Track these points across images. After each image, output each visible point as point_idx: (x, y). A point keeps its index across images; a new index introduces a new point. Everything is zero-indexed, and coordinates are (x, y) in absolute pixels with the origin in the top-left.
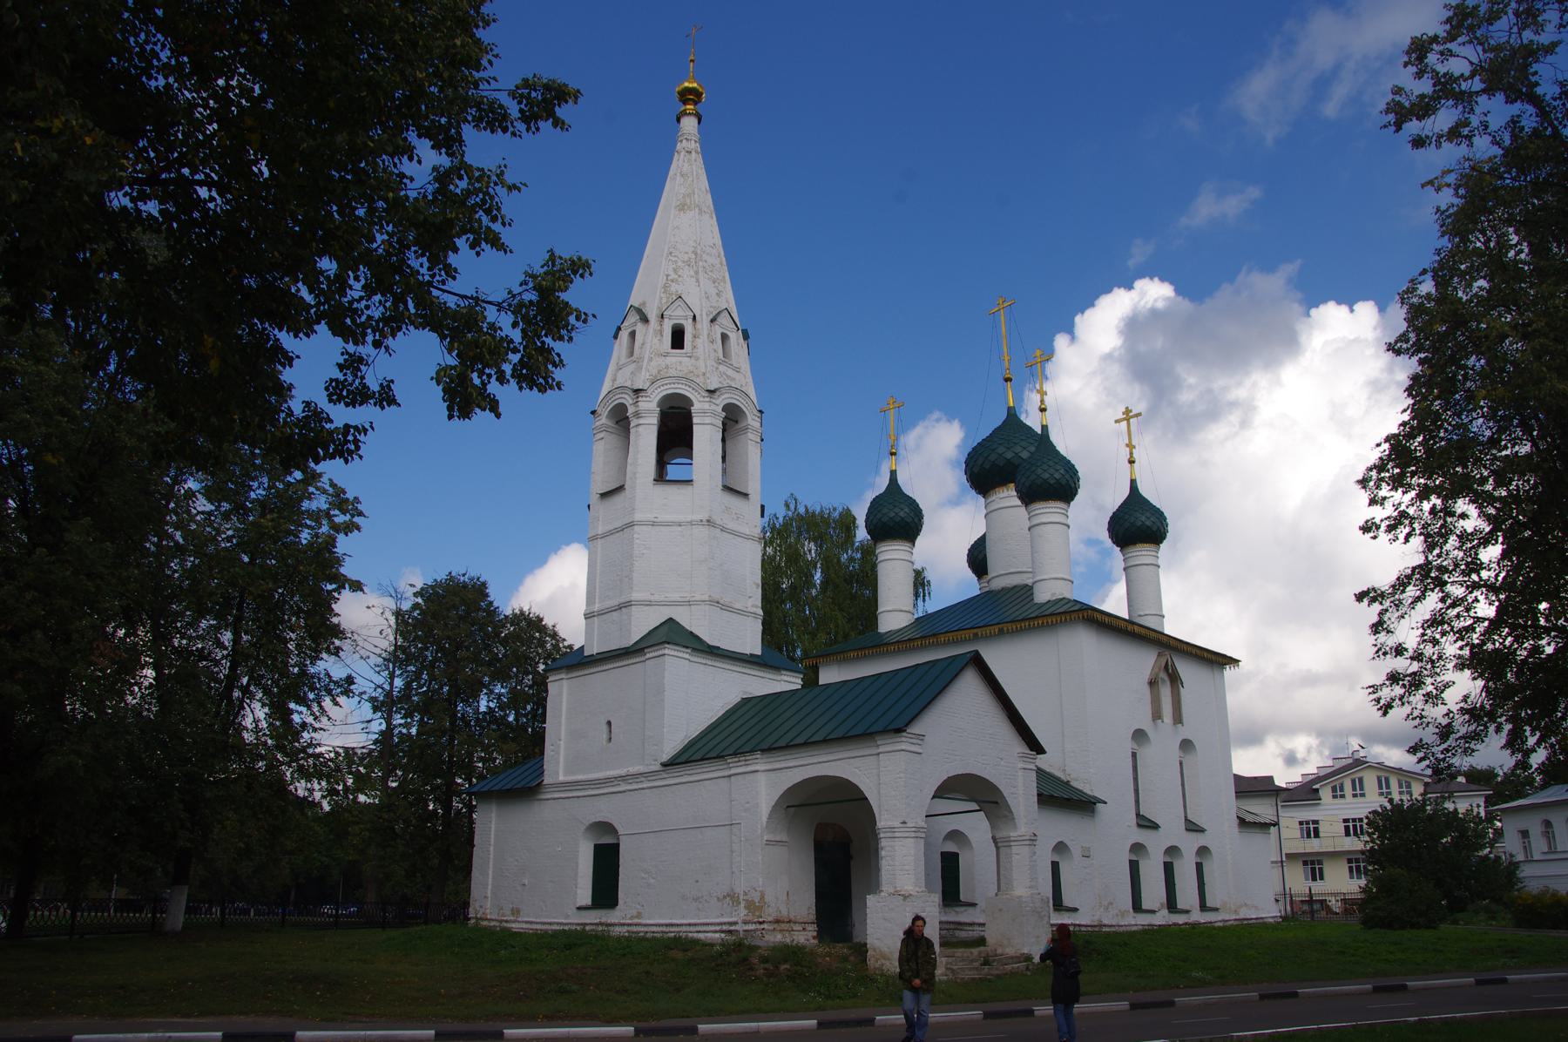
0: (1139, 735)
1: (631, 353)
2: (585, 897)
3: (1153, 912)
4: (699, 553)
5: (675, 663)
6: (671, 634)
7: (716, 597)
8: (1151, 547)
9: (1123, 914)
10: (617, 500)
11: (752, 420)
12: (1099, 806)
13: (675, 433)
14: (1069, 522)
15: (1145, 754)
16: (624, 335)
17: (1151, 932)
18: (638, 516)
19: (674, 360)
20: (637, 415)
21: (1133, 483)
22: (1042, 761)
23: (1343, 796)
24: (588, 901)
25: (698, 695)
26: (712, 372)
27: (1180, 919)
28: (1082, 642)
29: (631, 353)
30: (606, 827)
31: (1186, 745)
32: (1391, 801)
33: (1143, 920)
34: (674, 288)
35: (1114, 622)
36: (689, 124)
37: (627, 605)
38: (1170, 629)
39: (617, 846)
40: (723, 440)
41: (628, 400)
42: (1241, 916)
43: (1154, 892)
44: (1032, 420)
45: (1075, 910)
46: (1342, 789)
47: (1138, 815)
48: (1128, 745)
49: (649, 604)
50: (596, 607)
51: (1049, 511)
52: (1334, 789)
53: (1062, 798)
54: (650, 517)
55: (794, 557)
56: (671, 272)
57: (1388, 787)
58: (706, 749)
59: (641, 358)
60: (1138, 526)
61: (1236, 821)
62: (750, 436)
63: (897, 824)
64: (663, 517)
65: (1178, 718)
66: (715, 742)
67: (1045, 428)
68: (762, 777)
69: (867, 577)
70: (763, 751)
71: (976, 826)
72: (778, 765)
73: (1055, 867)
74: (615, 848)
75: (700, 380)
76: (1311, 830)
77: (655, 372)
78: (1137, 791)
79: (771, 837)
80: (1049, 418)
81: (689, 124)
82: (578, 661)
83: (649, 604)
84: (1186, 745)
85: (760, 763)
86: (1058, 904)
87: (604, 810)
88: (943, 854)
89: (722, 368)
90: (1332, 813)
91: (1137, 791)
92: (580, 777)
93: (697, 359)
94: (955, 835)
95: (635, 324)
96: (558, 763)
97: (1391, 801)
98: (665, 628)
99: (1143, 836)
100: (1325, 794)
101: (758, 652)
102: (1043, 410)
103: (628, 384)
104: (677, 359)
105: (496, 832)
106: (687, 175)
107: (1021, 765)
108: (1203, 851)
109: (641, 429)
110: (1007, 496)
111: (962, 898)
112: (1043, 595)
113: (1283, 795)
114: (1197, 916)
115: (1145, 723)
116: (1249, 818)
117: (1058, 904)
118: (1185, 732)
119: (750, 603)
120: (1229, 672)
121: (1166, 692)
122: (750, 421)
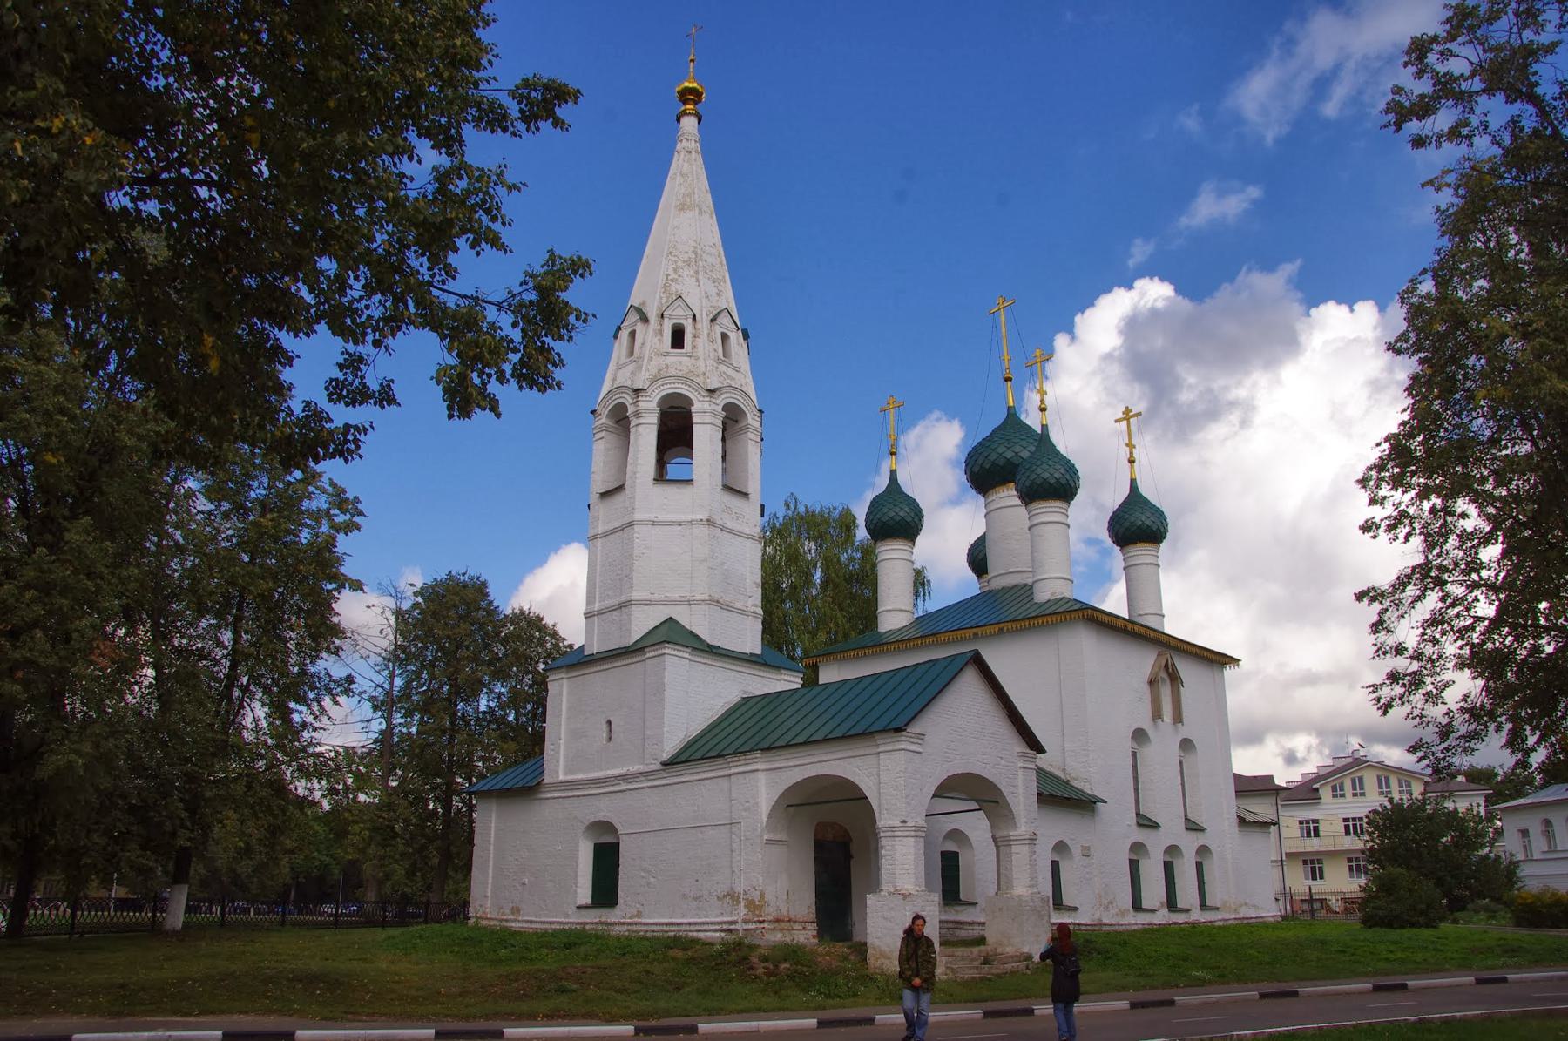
0: (1139, 735)
1: (631, 353)
2: (584, 894)
3: (1153, 911)
4: (699, 551)
5: (676, 665)
6: (671, 634)
7: (716, 596)
8: (1151, 546)
9: (1123, 913)
10: (618, 499)
11: (752, 420)
13: (675, 433)
14: (1069, 521)
15: (1148, 753)
20: (637, 414)
21: (1133, 482)
22: (1042, 760)
23: (1343, 796)
24: (588, 901)
25: (696, 696)
26: (715, 371)
27: (1180, 918)
28: (1083, 644)
29: (631, 353)
30: (605, 826)
31: (1186, 745)
32: (1391, 800)
33: (1143, 919)
36: (689, 123)
37: (628, 604)
38: (1172, 628)
40: (723, 439)
41: (628, 399)
43: (1154, 892)
44: (1032, 420)
45: (1076, 909)
46: (1342, 789)
47: (1138, 814)
48: (1128, 745)
49: (649, 603)
50: (597, 606)
51: (1048, 510)
52: (1334, 789)
53: (1062, 797)
56: (671, 271)
57: (1388, 786)
59: (642, 358)
60: (1138, 526)
61: (1236, 820)
62: (750, 435)
63: (897, 823)
64: (662, 517)
65: (1178, 718)
67: (1044, 427)
68: (762, 778)
69: (867, 577)
71: (976, 826)
73: (1055, 865)
74: (615, 848)
76: (1311, 829)
77: (654, 371)
78: (1136, 790)
81: (689, 123)
82: (579, 661)
83: (649, 603)
84: (1186, 745)
85: (760, 763)
87: (603, 809)
88: (943, 854)
89: (722, 368)
90: (1332, 812)
91: (1136, 790)
92: (580, 776)
94: (956, 835)
95: (635, 324)
96: (559, 762)
97: (1391, 800)
100: (1325, 793)
102: (1043, 410)
103: (628, 383)
106: (687, 173)
107: (1021, 764)
108: (1203, 850)
109: (641, 428)
112: (1043, 594)
113: (1283, 795)
114: (1197, 916)
115: (1146, 724)
116: (1249, 817)
118: (1185, 731)
119: (750, 602)
120: (1229, 672)
122: (750, 421)
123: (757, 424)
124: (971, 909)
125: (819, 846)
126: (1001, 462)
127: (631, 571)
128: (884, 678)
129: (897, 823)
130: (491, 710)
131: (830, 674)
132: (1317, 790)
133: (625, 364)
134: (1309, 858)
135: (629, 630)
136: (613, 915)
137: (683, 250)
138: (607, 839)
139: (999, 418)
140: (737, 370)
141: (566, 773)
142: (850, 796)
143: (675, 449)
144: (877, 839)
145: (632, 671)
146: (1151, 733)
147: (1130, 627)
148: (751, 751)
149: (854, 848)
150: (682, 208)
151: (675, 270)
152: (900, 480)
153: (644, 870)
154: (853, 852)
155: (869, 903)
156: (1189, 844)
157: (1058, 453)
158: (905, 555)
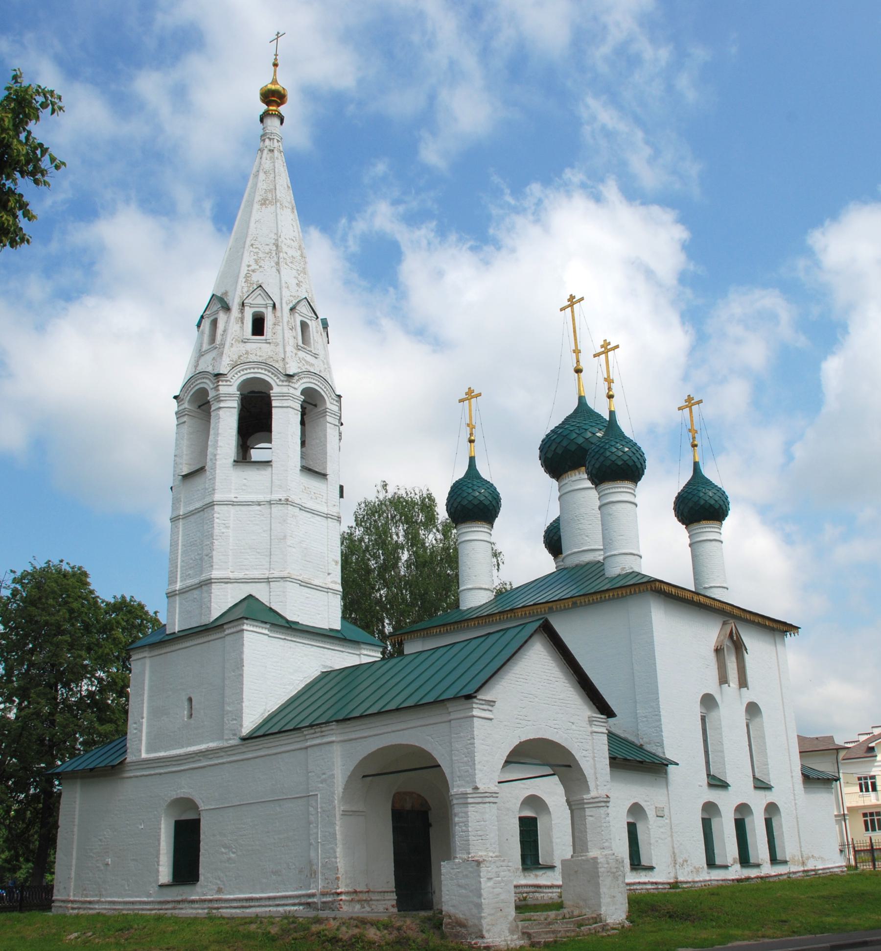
0: (708, 702)
1: (213, 339)
2: (165, 873)
3: (726, 867)
5: (256, 641)
6: (252, 611)
9: (698, 871)
10: (198, 483)
12: (671, 768)
14: (636, 501)
17: (715, 892)
18: (217, 497)
19: (254, 346)
20: (218, 399)
22: (618, 725)
25: (272, 674)
27: (753, 873)
29: (213, 339)
30: (187, 803)
31: (753, 709)
33: (717, 875)
34: (256, 278)
35: (681, 593)
37: (208, 582)
40: (303, 423)
41: (209, 385)
42: (810, 866)
43: (728, 848)
44: (601, 408)
45: (651, 868)
47: (709, 775)
48: (697, 710)
49: (227, 581)
50: (178, 586)
51: (619, 491)
54: (231, 496)
55: (382, 538)
56: (252, 263)
58: (283, 723)
59: (223, 345)
62: (329, 419)
63: (469, 790)
64: (243, 498)
65: (743, 683)
66: (291, 716)
67: (612, 413)
68: (337, 749)
69: (450, 557)
70: (337, 721)
71: (551, 790)
72: (353, 736)
75: (279, 365)
77: (235, 357)
79: (347, 808)
80: (617, 405)
82: (167, 640)
83: (227, 581)
85: (334, 734)
86: (636, 863)
87: (185, 788)
88: (521, 819)
89: (301, 354)
92: (162, 754)
93: (277, 345)
94: (533, 801)
95: (217, 312)
96: (141, 743)
99: (715, 796)
101: (337, 625)
102: (610, 397)
103: (210, 369)
104: (258, 349)
105: (78, 810)
108: (772, 809)
109: (221, 412)
110: (580, 480)
111: (717, 863)
114: (767, 870)
115: (712, 687)
116: (813, 775)
117: (636, 863)
118: (749, 696)
119: (329, 579)
122: (328, 405)
124: (550, 873)
125: (398, 816)
126: (573, 448)
127: (212, 550)
129: (469, 790)
130: (91, 694)
132: (872, 749)
133: (207, 351)
134: (868, 811)
135: (209, 608)
136: (194, 893)
138: (189, 816)
139: (572, 406)
141: (148, 751)
142: (427, 766)
143: (258, 435)
145: (212, 646)
147: (696, 598)
148: (327, 723)
150: (264, 202)
151: (256, 261)
153: (225, 847)
154: (431, 820)
155: (443, 870)
156: (758, 802)
157: (625, 437)
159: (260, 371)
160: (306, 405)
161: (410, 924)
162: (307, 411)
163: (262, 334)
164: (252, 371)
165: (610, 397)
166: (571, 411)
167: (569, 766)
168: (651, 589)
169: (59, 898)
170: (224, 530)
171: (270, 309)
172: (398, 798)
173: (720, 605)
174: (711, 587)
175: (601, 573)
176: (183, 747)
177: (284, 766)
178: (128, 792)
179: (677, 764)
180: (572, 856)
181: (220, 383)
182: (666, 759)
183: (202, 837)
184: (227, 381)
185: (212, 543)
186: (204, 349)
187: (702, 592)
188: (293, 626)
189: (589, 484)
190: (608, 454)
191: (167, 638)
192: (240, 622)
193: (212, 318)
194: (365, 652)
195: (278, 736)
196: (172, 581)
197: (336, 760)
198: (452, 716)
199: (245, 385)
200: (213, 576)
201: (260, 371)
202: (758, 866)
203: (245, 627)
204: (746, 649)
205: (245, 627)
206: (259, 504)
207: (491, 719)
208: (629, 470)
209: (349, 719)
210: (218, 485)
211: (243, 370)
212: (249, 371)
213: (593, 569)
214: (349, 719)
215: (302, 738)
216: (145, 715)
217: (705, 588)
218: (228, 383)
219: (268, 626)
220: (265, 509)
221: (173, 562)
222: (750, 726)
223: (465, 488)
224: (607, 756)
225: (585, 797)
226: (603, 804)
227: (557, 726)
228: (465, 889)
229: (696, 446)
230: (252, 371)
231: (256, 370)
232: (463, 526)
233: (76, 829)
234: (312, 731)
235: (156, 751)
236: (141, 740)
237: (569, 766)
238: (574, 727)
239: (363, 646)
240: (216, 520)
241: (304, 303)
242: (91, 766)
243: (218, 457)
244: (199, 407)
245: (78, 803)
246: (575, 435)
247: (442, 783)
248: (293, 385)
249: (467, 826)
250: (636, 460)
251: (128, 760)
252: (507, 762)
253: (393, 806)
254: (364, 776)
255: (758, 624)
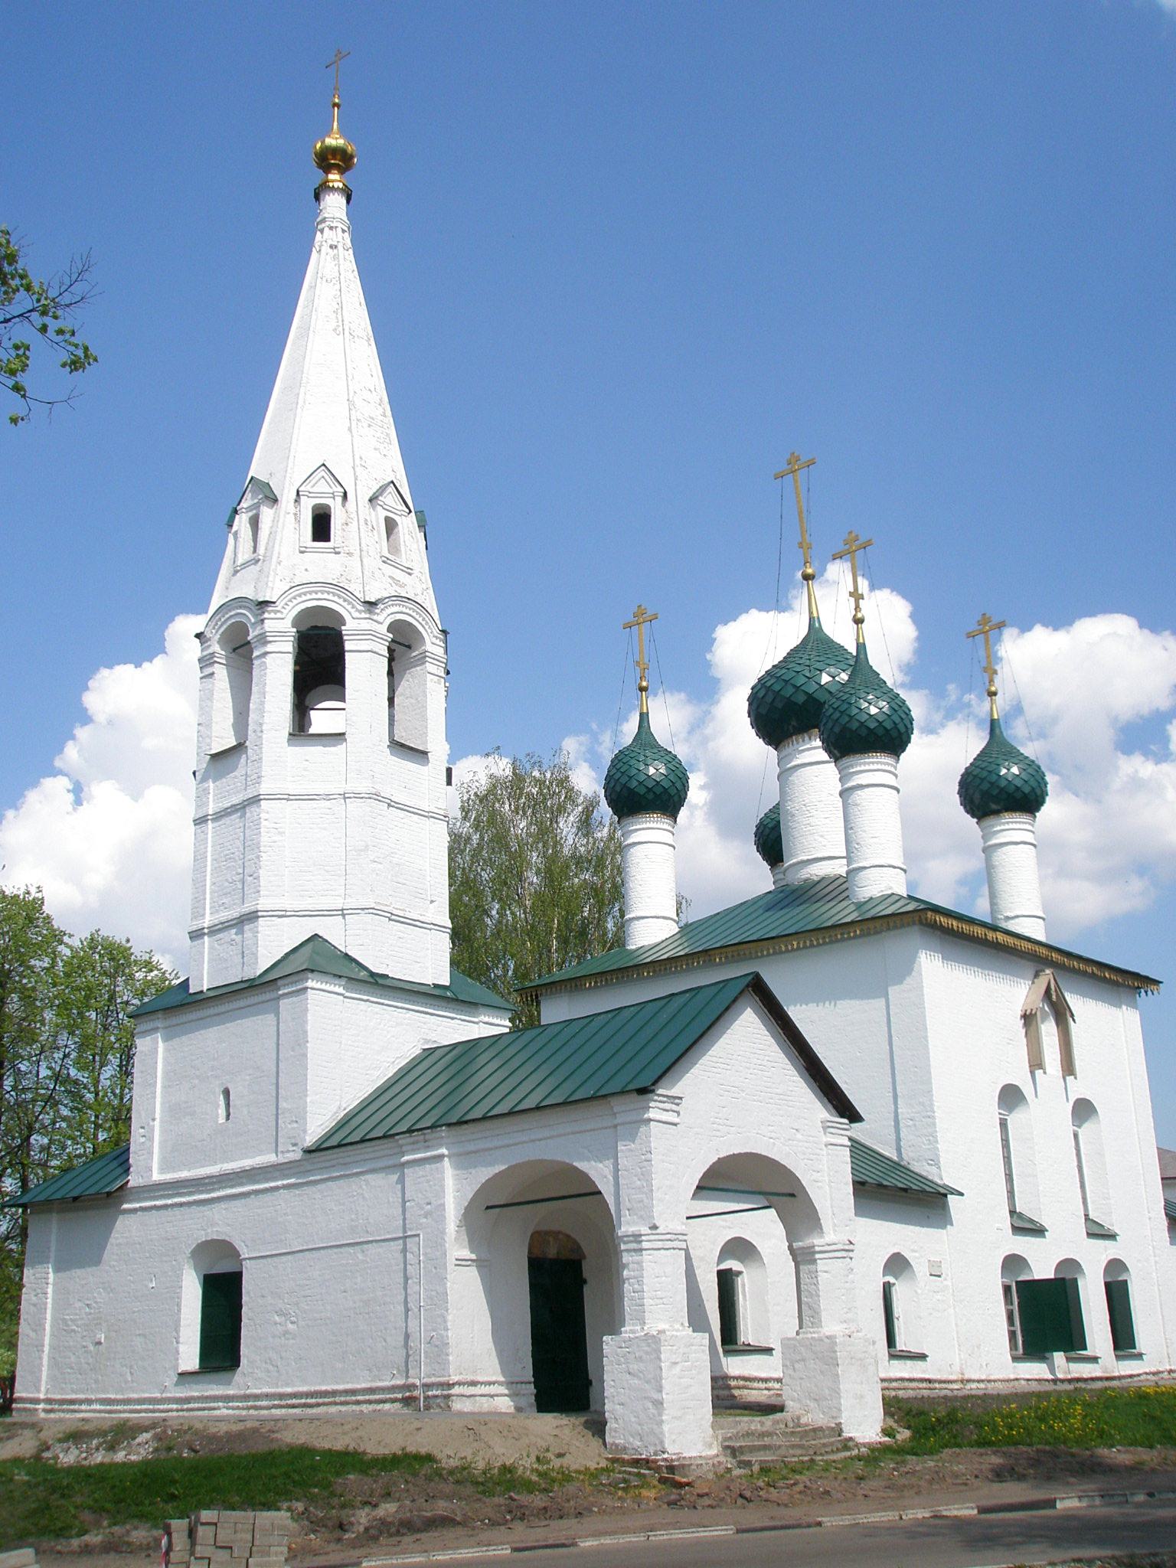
0: (1011, 1096)
2: (190, 1356)
4: (365, 841)
5: (324, 1003)
6: (318, 960)
11: (432, 645)
13: (320, 664)
16: (242, 522)
18: (264, 788)
20: (263, 639)
25: (354, 1050)
26: (379, 572)
30: (224, 1248)
31: (1083, 1110)
36: (334, 205)
39: (241, 1273)
44: (843, 635)
45: (922, 1357)
47: (1012, 1212)
48: (994, 1111)
50: (207, 921)
51: (872, 768)
53: (898, 1190)
62: (429, 667)
63: (645, 1230)
64: (480, 1379)
67: (861, 647)
70: (449, 1125)
71: (764, 1228)
75: (355, 588)
81: (334, 205)
82: (178, 1004)
84: (1083, 1110)
87: (221, 1222)
92: (184, 1174)
94: (740, 1248)
95: (257, 506)
96: (152, 1159)
98: (310, 945)
99: (1023, 1246)
102: (859, 621)
104: (324, 563)
106: (332, 292)
108: (1115, 1266)
109: (269, 659)
110: (812, 750)
118: (1079, 1088)
121: (1049, 1030)
122: (429, 647)
123: (440, 651)
125: (537, 1266)
126: (801, 699)
127: (258, 867)
128: (626, 1014)
129: (645, 1230)
131: (554, 1011)
135: (255, 955)
137: (330, 397)
140: (409, 571)
143: (321, 689)
144: (618, 1253)
146: (1027, 1090)
147: (991, 935)
149: (587, 1271)
152: (654, 729)
155: (606, 1349)
158: (667, 837)
159: (325, 596)
160: (394, 646)
161: (555, 1429)
162: (395, 654)
163: (328, 539)
164: (314, 596)
165: (859, 621)
166: (795, 642)
167: (793, 1195)
168: (921, 923)
169: (24, 1395)
170: (275, 838)
171: (339, 500)
172: (538, 1239)
173: (1030, 946)
174: (1017, 917)
175: (844, 895)
176: (216, 1163)
177: (365, 1197)
178: (130, 1229)
179: (962, 1194)
180: (798, 1333)
181: (266, 615)
182: (945, 1187)
183: (245, 1299)
184: (276, 612)
185: (258, 857)
186: (240, 561)
187: (1004, 925)
188: (380, 981)
189: (823, 756)
190: (855, 711)
191: (190, 999)
192: (301, 976)
193: (251, 514)
194: (486, 1019)
195: (359, 1146)
196: (198, 914)
197: (449, 1183)
198: (619, 1120)
199: (315, 508)
200: (259, 907)
201: (325, 596)
202: (1094, 1359)
203: (310, 984)
204: (1072, 1015)
205: (310, 984)
206: (328, 797)
207: (675, 1125)
208: (890, 737)
209: (466, 1122)
210: (266, 770)
211: (300, 595)
212: (309, 597)
213: (831, 888)
214: (466, 1122)
215: (396, 1150)
216: (157, 1116)
217: (1008, 918)
218: (279, 615)
219: (343, 982)
220: (338, 805)
221: (198, 884)
222: (1080, 1137)
223: (633, 762)
224: (849, 1178)
225: (816, 1241)
226: (843, 1254)
227: (773, 1135)
228: (639, 1378)
229: (995, 694)
230: (314, 596)
231: (319, 596)
232: (631, 820)
233: (50, 1290)
234: (411, 1140)
235: (174, 1170)
236: (151, 1153)
237: (793, 1195)
238: (799, 1136)
239: (481, 1009)
240: (264, 823)
241: (391, 488)
242: (75, 1193)
243: (264, 727)
244: (234, 650)
245: (53, 1249)
246: (803, 680)
247: (603, 1221)
248: (375, 617)
249: (640, 1283)
250: (898, 720)
251: (130, 1185)
252: (695, 1196)
253: (530, 1252)
254: (488, 1208)
255: (1093, 976)
